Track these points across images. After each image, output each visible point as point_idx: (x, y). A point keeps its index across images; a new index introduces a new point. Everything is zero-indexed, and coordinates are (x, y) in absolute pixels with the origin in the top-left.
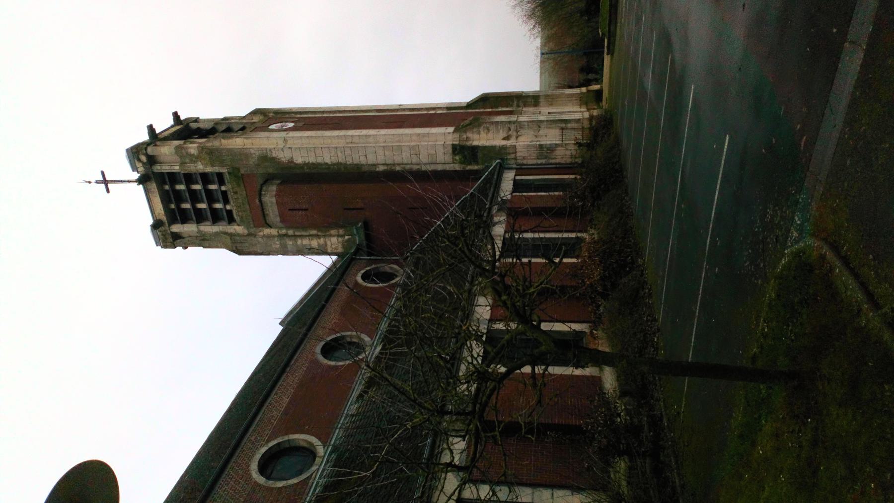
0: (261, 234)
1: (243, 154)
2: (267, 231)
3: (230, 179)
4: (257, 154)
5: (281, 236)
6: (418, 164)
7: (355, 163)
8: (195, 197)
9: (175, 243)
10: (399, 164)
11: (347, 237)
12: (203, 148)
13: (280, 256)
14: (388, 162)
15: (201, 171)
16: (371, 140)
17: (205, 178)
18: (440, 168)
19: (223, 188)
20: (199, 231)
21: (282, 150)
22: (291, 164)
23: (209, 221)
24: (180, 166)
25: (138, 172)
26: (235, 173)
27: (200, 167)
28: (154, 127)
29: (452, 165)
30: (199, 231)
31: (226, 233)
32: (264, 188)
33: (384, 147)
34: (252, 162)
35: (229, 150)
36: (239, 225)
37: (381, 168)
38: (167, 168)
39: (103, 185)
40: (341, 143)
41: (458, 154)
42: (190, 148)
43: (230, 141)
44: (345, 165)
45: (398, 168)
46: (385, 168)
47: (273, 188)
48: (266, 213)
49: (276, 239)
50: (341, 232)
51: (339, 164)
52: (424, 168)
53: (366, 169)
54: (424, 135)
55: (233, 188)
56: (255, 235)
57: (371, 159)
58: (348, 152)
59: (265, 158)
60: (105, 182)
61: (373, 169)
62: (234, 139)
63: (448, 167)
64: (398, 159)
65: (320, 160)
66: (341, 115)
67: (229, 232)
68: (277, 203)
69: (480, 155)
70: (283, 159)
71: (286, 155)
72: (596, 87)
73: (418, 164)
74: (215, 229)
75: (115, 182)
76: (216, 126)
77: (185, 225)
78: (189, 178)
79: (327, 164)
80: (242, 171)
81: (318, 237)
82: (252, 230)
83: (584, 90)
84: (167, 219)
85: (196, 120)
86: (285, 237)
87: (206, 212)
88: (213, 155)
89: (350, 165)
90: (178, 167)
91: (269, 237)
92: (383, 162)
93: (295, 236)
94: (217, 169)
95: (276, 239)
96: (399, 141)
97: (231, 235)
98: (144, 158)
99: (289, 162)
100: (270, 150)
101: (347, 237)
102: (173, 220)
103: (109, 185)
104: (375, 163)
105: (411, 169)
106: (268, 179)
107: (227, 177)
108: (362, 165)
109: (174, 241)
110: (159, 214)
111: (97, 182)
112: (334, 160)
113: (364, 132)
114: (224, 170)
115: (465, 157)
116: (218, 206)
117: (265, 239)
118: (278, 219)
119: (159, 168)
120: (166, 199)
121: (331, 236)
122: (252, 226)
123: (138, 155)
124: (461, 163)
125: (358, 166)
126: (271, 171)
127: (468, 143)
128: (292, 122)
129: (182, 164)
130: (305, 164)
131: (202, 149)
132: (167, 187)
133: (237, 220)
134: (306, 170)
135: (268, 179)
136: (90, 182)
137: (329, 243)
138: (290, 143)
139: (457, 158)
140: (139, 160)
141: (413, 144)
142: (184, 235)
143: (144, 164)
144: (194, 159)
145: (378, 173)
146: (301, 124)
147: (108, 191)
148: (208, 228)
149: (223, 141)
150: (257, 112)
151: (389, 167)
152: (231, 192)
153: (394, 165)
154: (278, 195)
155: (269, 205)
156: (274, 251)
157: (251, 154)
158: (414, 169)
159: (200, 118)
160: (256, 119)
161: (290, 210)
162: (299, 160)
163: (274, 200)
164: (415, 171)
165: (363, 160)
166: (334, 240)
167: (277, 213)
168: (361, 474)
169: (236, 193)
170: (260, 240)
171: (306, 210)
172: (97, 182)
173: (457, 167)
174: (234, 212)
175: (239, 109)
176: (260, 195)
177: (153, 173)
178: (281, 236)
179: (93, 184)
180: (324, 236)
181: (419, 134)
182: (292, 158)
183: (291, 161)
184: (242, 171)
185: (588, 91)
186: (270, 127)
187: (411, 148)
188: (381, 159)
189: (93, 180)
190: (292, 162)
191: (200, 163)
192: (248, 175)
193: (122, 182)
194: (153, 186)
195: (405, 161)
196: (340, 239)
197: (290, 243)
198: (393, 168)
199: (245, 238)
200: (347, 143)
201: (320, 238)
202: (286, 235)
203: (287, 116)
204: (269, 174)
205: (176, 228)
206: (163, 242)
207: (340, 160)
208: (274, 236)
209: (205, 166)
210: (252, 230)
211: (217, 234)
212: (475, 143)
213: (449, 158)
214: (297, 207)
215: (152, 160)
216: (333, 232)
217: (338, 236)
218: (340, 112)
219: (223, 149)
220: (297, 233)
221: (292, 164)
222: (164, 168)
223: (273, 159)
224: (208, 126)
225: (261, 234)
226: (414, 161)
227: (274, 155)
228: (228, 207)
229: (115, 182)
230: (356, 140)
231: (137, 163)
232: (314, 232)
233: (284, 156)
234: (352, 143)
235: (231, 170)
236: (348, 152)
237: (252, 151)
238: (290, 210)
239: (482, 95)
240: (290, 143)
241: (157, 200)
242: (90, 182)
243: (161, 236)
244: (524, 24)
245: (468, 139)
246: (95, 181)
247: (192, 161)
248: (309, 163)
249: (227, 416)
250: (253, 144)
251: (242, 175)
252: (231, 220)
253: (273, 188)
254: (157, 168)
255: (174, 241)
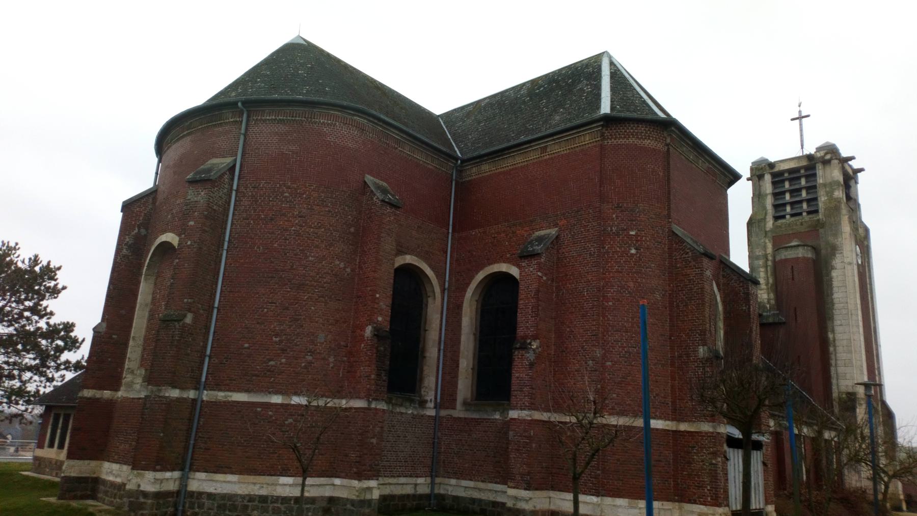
0: (767, 241)
1: (837, 233)
2: (770, 246)
3: (814, 220)
4: (837, 243)
5: (765, 257)
6: (836, 365)
7: (835, 316)
8: (795, 192)
10: (835, 350)
11: (768, 306)
12: (838, 202)
13: (748, 253)
14: (837, 342)
15: (819, 198)
17: (813, 201)
18: (834, 381)
19: (804, 214)
20: (766, 195)
23: (775, 201)
25: (815, 152)
26: (819, 225)
27: (823, 199)
29: (837, 391)
30: (766, 195)
31: (766, 214)
32: (809, 248)
33: (850, 339)
34: (831, 239)
35: (839, 223)
36: (773, 224)
37: (831, 336)
38: (821, 173)
39: (797, 116)
40: (851, 307)
41: (848, 397)
42: (839, 192)
43: (847, 222)
45: (831, 349)
46: (831, 339)
47: (810, 255)
48: (789, 249)
49: (764, 252)
50: (773, 302)
51: (833, 304)
52: (833, 369)
53: (829, 324)
54: (862, 371)
55: (805, 222)
57: (838, 329)
58: (844, 312)
59: (834, 250)
60: (801, 118)
61: (830, 328)
62: (848, 225)
63: (834, 387)
64: (840, 349)
65: (835, 289)
66: (870, 299)
67: (767, 217)
68: (798, 258)
69: (848, 414)
70: (834, 262)
71: (838, 265)
72: (904, 507)
73: (836, 365)
74: (769, 207)
75: (801, 125)
76: (853, 200)
77: (771, 185)
78: (812, 188)
79: (833, 295)
80: (821, 231)
81: (767, 284)
82: (769, 234)
83: (902, 497)
84: (777, 172)
85: (856, 183)
86: (765, 259)
87: (782, 198)
88: (835, 210)
89: (833, 313)
91: (765, 248)
92: (837, 338)
93: (766, 267)
94: (821, 211)
95: (764, 252)
96: (855, 351)
97: (765, 219)
98: (828, 157)
99: (832, 266)
101: (768, 306)
102: (774, 175)
104: (835, 332)
105: (832, 359)
106: (816, 249)
107: (814, 217)
110: (780, 166)
111: (800, 112)
112: (836, 301)
114: (821, 216)
116: (788, 209)
117: (763, 244)
118: (783, 257)
119: (820, 168)
121: (768, 294)
122: (774, 235)
124: (840, 398)
125: (832, 319)
126: (823, 252)
128: (862, 262)
129: (825, 185)
130: (831, 280)
131: (839, 201)
132: (802, 171)
134: (825, 279)
135: (816, 249)
136: (799, 106)
137: (762, 292)
138: (849, 267)
139: (844, 396)
140: (826, 154)
141: (854, 362)
142: (761, 182)
144: (830, 194)
146: (861, 269)
147: (793, 119)
148: (769, 201)
149: (847, 217)
150: (867, 230)
151: (832, 342)
152: (801, 220)
153: (835, 346)
154: (805, 259)
155: (796, 252)
156: (752, 249)
157: (837, 238)
158: (831, 361)
160: (861, 231)
161: (792, 267)
162: (834, 274)
163: (800, 255)
164: (829, 362)
165: (837, 322)
166: (765, 296)
167: (789, 257)
168: (375, 183)
171: (793, 279)
172: (800, 112)
173: (835, 395)
174: (783, 221)
175: (867, 217)
176: (804, 246)
177: (816, 163)
178: (765, 257)
179: (798, 109)
180: (768, 289)
181: (862, 367)
182: (836, 269)
183: (833, 268)
184: (821, 231)
185: (901, 500)
186: (857, 246)
187: (850, 360)
188: (839, 336)
189: (801, 108)
191: (826, 198)
194: (804, 163)
195: (838, 355)
197: (761, 262)
198: (832, 345)
199: (763, 229)
200: (851, 311)
202: (767, 260)
203: (866, 256)
205: (768, 178)
206: (756, 168)
208: (765, 251)
209: (824, 203)
210: (769, 234)
211: (764, 208)
212: (858, 410)
213: (843, 389)
214: (795, 273)
215: (826, 163)
216: (772, 296)
217: (769, 300)
218: (872, 298)
219: (840, 218)
221: (830, 268)
222: (821, 171)
223: (834, 255)
224: (852, 195)
225: (767, 241)
226: (839, 362)
227: (837, 255)
228: (788, 217)
229: (801, 125)
230: (854, 317)
231: (825, 152)
232: (771, 281)
233: (837, 262)
234: (851, 315)
235: (821, 222)
236: (844, 312)
237: (840, 240)
238: (792, 267)
239: (894, 414)
240: (849, 267)
241: (792, 165)
243: (761, 167)
245: (861, 405)
246: (801, 109)
247: (827, 193)
248: (832, 281)
250: (845, 239)
251: (818, 230)
252: (776, 218)
253: (810, 255)
254: (819, 167)
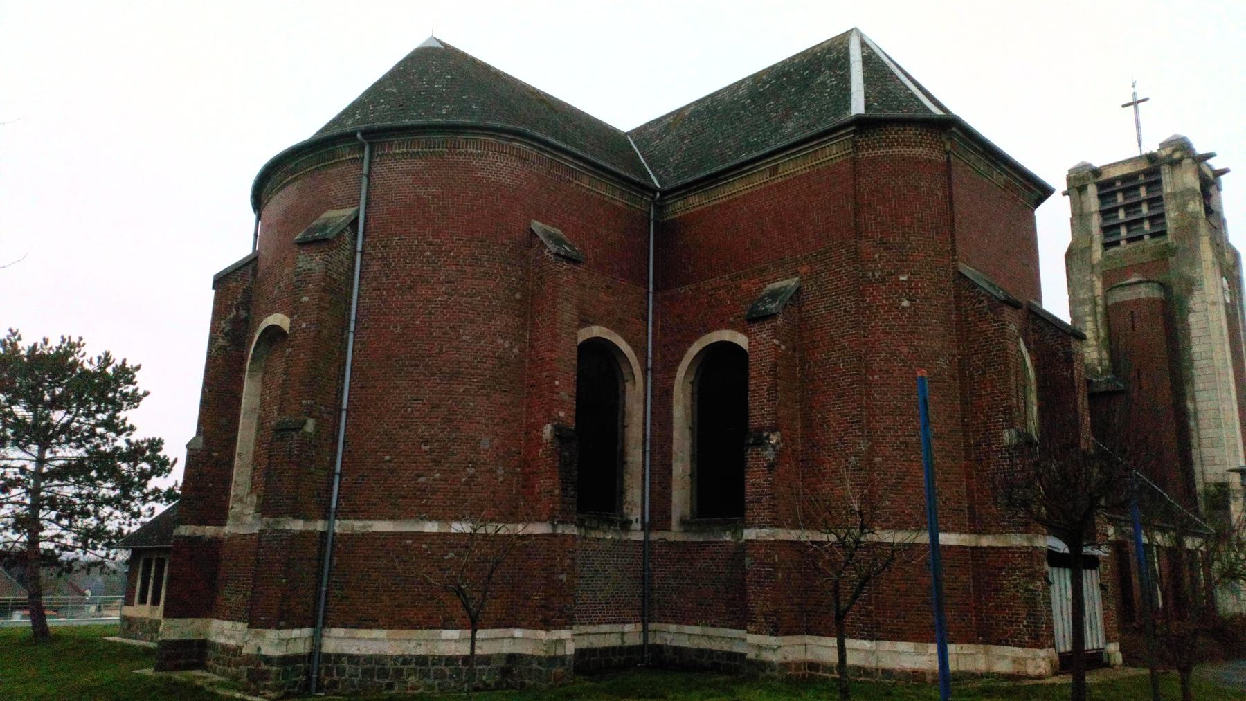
0: (1095, 278)
1: (1194, 262)
8: (1131, 208)
9: (1075, 190)
10: (1197, 425)
11: (1099, 368)
16: (1225, 395)
17: (1157, 219)
18: (1197, 468)
19: (1147, 237)
21: (1203, 302)
22: (1184, 311)
24: (1171, 193)
25: (1159, 150)
26: (1165, 253)
27: (1172, 215)
28: (1227, 174)
29: (1201, 481)
31: (1091, 241)
32: (1155, 285)
34: (1186, 270)
37: (1190, 406)
40: (1218, 363)
44: (1191, 367)
45: (1192, 424)
47: (1156, 294)
50: (1106, 363)
51: (1191, 361)
56: (1092, 272)
57: (1201, 396)
58: (1208, 371)
59: (1191, 285)
63: (1198, 478)
65: (1194, 341)
70: (1192, 302)
73: (1199, 445)
75: (1136, 113)
78: (1155, 201)
84: (1105, 180)
85: (1219, 189)
90: (1169, 191)
92: (1199, 408)
94: (1170, 232)
97: (1090, 247)
98: (1177, 155)
100: (1201, 289)
102: (1101, 186)
103: (1132, 107)
106: (1165, 286)
107: (1161, 241)
108: (1193, 386)
109: (1077, 188)
111: (1134, 94)
112: (1196, 356)
113: (1233, 386)
114: (1170, 239)
115: (1214, 496)
119: (1167, 171)
120: (1125, 178)
121: (1100, 353)
123: (1182, 150)
125: (1190, 381)
126: (1176, 289)
127: (1232, 501)
128: (1231, 301)
129: (1174, 195)
131: (1194, 216)
133: (1108, 251)
135: (1165, 286)
136: (1133, 86)
138: (1212, 309)
140: (1174, 151)
143: (1170, 156)
144: (1182, 208)
145: (1185, 401)
148: (1095, 223)
150: (1236, 255)
153: (1196, 419)
159: (1222, 192)
160: (1228, 256)
161: (1132, 312)
162: (1192, 319)
163: (1143, 296)
166: (1095, 355)
169: (1143, 251)
170: (1088, 278)
172: (1134, 94)
173: (1199, 487)
179: (1132, 90)
182: (1194, 311)
184: (1171, 259)
187: (1220, 438)
188: (1201, 405)
189: (1136, 89)
190: (1189, 312)
192: (1166, 266)
193: (1137, 120)
194: (1144, 166)
196: (1096, 361)
197: (1087, 308)
201: (1095, 340)
202: (1096, 304)
204: (1171, 287)
205: (1092, 190)
206: (1075, 177)
207: (1197, 363)
210: (1098, 270)
211: (1089, 232)
212: (1232, 507)
213: (1211, 478)
214: (1137, 320)
216: (1105, 354)
217: (1100, 360)
220: (1099, 316)
223: (1190, 292)
224: (1214, 206)
225: (1095, 278)
226: (1204, 442)
227: (1196, 293)
228: (1123, 243)
229: (1136, 113)
233: (1196, 302)
237: (1198, 270)
238: (1132, 312)
240: (1212, 309)
242: (1133, 86)
244: (75, 340)
249: (667, 130)
251: (1167, 260)
252: (1106, 246)
253: (1156, 294)
254: (1165, 170)
255: (1077, 188)
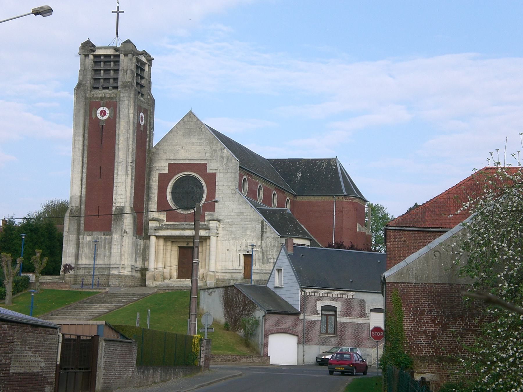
111: (118, 7)
172: (118, 7)
